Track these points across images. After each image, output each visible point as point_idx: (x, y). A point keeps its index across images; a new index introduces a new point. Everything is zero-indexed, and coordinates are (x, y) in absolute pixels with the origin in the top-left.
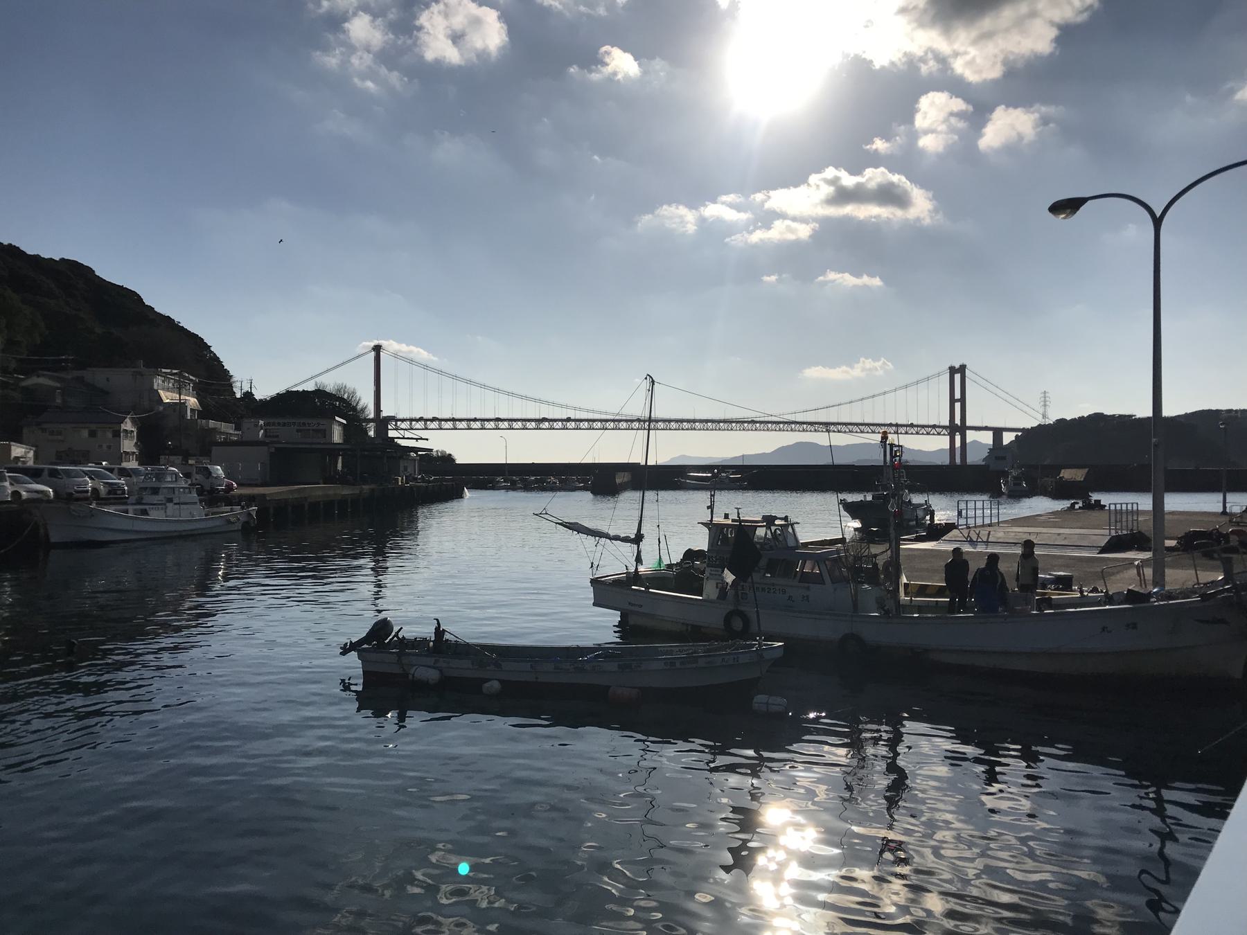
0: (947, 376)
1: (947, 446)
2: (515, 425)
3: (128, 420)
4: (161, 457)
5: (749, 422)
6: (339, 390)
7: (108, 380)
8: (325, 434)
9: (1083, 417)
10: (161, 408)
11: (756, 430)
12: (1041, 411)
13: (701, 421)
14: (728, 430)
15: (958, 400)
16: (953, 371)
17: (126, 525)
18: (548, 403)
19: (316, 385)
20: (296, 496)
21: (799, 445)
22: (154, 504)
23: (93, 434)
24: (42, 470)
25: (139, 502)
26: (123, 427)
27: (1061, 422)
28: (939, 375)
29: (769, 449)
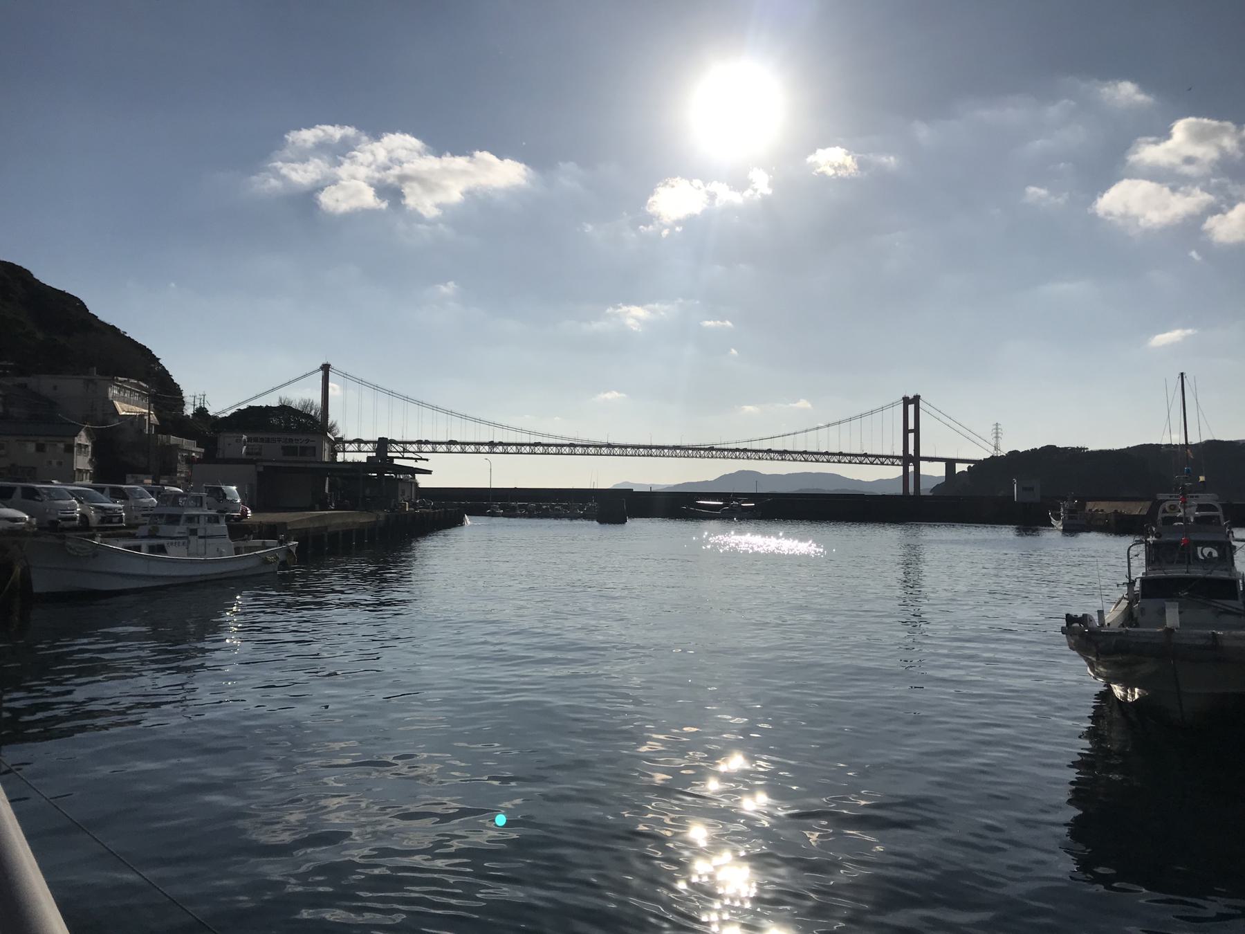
0: (902, 406)
2: (468, 448)
3: (82, 433)
5: (693, 449)
6: (305, 407)
7: (55, 388)
8: (315, 451)
9: (1036, 449)
10: (117, 423)
11: (712, 457)
12: (993, 442)
15: (911, 431)
16: (906, 401)
17: (139, 568)
18: (502, 426)
19: (280, 400)
20: (317, 525)
22: (174, 538)
23: (40, 448)
24: (12, 489)
25: (152, 535)
26: (77, 440)
27: (1014, 454)
28: (893, 405)
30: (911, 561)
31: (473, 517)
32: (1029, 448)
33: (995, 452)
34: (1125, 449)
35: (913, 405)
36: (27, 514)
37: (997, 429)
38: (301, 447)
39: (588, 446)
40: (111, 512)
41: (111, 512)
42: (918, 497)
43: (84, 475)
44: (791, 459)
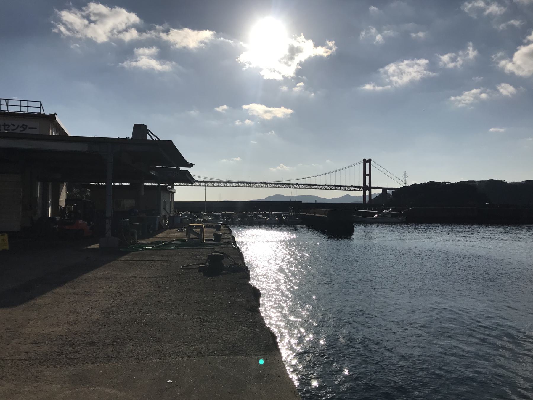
0: (362, 165)
1: (363, 195)
11: (256, 187)
12: (403, 180)
13: (253, 183)
15: (367, 175)
16: (365, 161)
28: (359, 163)
32: (422, 182)
33: (404, 184)
34: (454, 183)
35: (368, 163)
37: (405, 174)
44: (294, 187)
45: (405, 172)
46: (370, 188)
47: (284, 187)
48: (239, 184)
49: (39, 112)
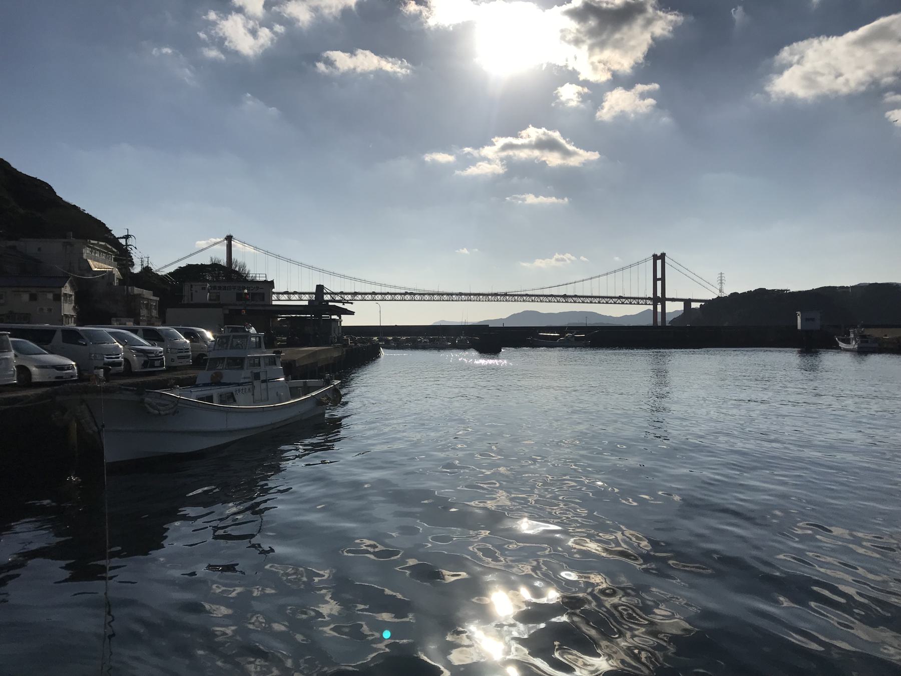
3: (67, 284)
4: (113, 319)
7: (39, 249)
12: (719, 287)
13: (475, 295)
14: (477, 301)
15: (659, 279)
16: (655, 257)
17: (215, 422)
18: (361, 280)
21: (526, 313)
23: (33, 297)
27: (734, 295)
28: (646, 260)
29: (505, 316)
30: (661, 374)
31: (387, 350)
36: (74, 361)
38: (252, 293)
39: (424, 294)
40: (153, 355)
41: (153, 355)
42: (663, 326)
43: (70, 319)
44: (556, 301)
45: (721, 274)
46: (663, 300)
47: (541, 301)
48: (454, 296)
49: (127, 234)
